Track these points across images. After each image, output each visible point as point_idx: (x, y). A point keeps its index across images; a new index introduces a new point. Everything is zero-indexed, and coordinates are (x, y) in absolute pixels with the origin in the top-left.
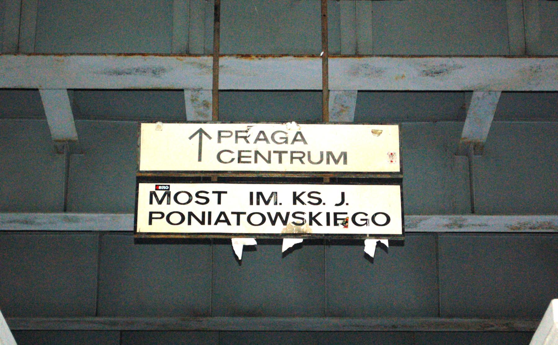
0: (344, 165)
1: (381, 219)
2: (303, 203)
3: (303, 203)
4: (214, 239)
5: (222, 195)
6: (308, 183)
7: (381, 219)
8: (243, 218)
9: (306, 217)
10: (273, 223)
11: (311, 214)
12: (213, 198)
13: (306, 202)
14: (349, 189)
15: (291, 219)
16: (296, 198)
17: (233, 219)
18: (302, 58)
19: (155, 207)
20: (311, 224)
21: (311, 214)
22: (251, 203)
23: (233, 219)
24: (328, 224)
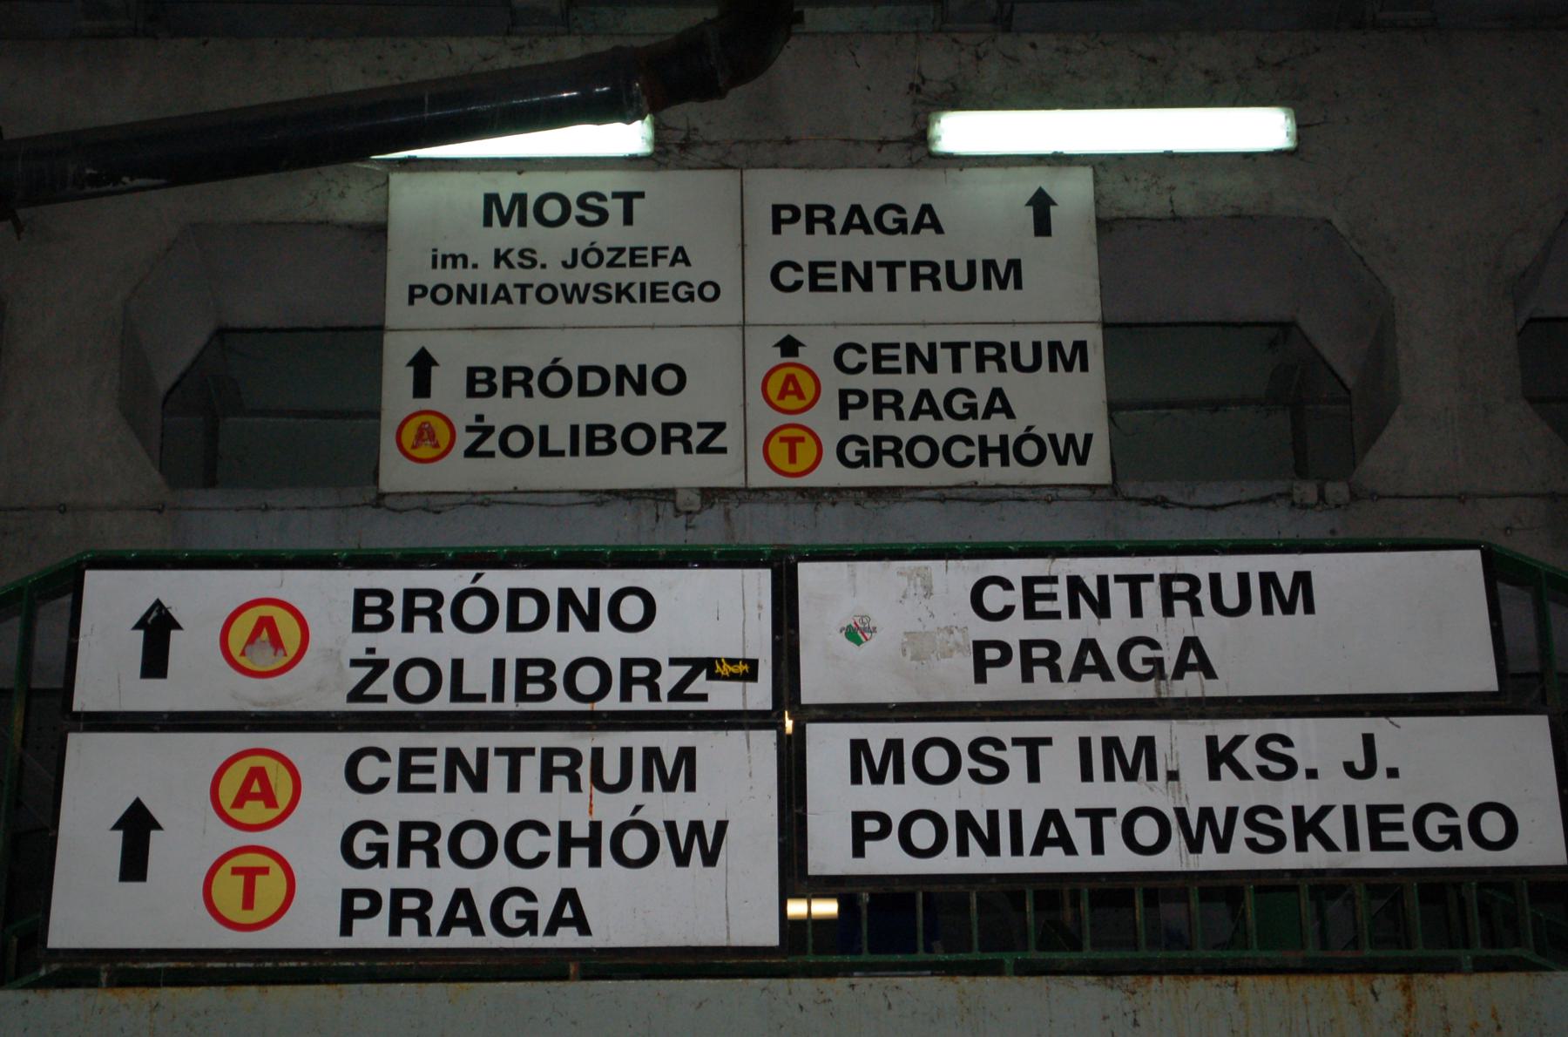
0: (984, 434)
1: (1493, 826)
2: (1242, 774)
3: (1242, 774)
4: (896, 970)
5: (1042, 750)
6: (420, 566)
7: (1493, 826)
8: (1112, 829)
9: (1287, 825)
10: (1195, 846)
11: (1298, 811)
12: (1016, 758)
13: (1251, 770)
14: (1392, 734)
15: (1241, 831)
16: (1219, 758)
17: (1080, 831)
18: (865, 170)
19: (870, 796)
20: (1301, 846)
21: (1298, 811)
22: (1087, 775)
23: (1080, 831)
24: (1353, 844)
